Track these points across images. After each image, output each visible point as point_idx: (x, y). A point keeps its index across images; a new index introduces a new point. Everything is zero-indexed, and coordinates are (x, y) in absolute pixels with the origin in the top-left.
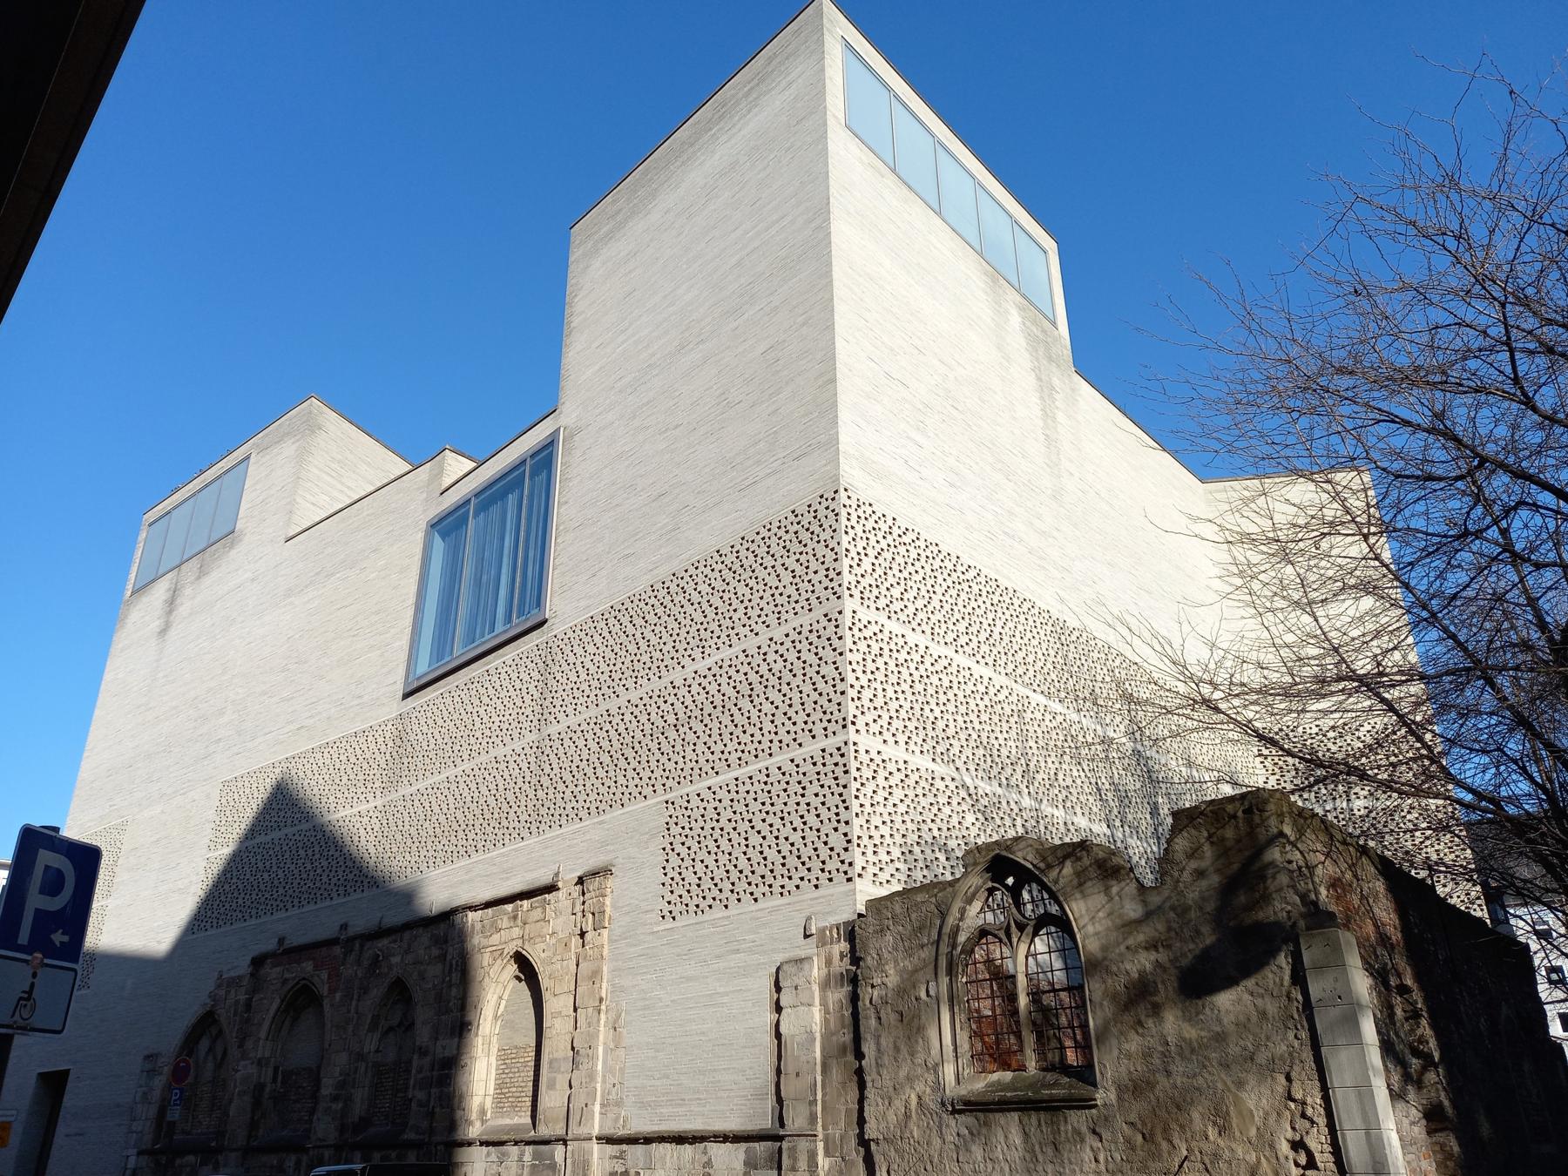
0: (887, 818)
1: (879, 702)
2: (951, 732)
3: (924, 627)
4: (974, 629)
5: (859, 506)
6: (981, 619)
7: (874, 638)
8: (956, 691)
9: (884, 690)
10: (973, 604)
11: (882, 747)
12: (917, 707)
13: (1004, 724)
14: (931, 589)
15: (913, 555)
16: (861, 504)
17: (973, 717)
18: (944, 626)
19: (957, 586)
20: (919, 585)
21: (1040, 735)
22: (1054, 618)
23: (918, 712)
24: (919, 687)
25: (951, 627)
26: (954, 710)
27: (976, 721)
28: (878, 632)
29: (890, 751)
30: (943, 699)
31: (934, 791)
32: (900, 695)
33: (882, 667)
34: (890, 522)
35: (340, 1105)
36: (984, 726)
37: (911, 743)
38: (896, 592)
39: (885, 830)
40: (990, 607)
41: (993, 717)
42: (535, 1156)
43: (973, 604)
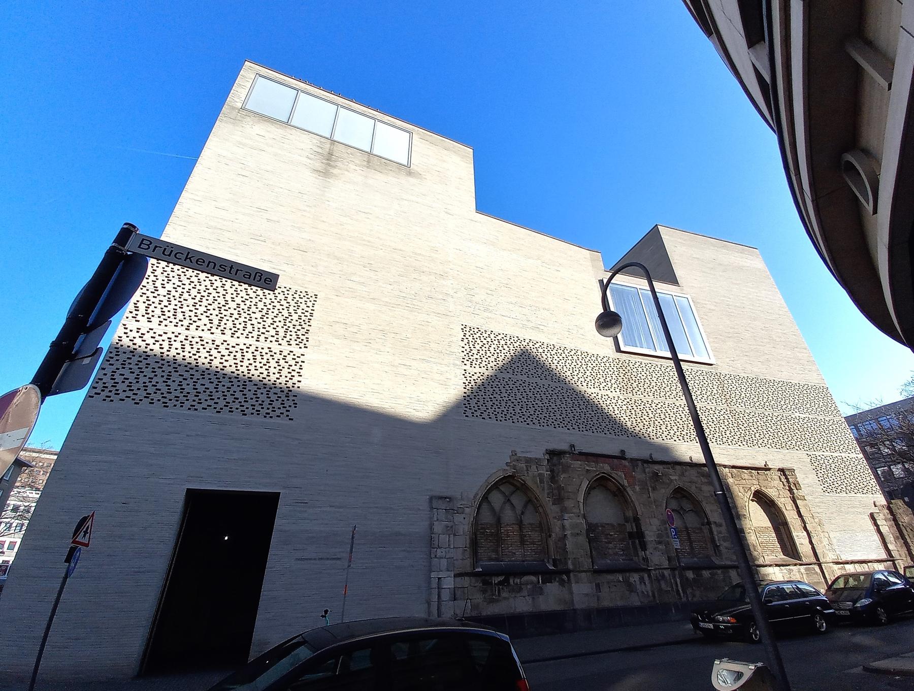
0: (833, 474)
1: (817, 440)
2: (842, 442)
3: (769, 407)
4: (787, 402)
5: (468, 343)
6: (707, 388)
7: (595, 398)
8: (814, 427)
9: (734, 429)
10: (702, 383)
11: (849, 455)
12: (717, 429)
13: (835, 432)
14: (712, 388)
15: (784, 389)
16: (614, 360)
17: (797, 431)
18: (802, 408)
19: (802, 393)
20: (707, 388)
21: (799, 427)
22: (768, 380)
23: (718, 431)
24: (827, 432)
25: (805, 407)
26: (841, 435)
27: (824, 434)
28: (596, 396)
29: (826, 454)
30: (836, 433)
31: (818, 460)
32: (823, 436)
33: (760, 425)
34: (798, 385)
35: (551, 568)
36: (802, 433)
37: (718, 441)
38: (782, 403)
39: (860, 478)
40: (710, 382)
41: (778, 427)
42: (806, 570)
43: (702, 383)
